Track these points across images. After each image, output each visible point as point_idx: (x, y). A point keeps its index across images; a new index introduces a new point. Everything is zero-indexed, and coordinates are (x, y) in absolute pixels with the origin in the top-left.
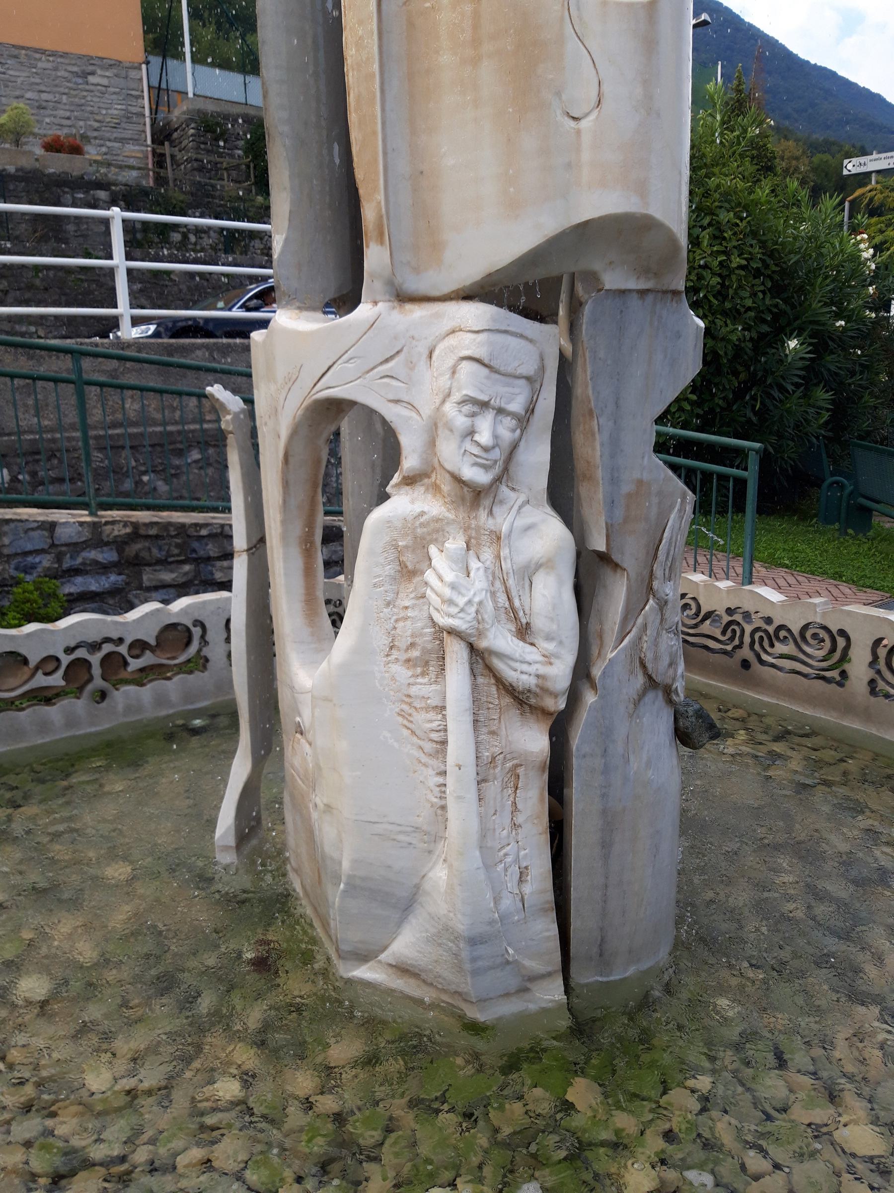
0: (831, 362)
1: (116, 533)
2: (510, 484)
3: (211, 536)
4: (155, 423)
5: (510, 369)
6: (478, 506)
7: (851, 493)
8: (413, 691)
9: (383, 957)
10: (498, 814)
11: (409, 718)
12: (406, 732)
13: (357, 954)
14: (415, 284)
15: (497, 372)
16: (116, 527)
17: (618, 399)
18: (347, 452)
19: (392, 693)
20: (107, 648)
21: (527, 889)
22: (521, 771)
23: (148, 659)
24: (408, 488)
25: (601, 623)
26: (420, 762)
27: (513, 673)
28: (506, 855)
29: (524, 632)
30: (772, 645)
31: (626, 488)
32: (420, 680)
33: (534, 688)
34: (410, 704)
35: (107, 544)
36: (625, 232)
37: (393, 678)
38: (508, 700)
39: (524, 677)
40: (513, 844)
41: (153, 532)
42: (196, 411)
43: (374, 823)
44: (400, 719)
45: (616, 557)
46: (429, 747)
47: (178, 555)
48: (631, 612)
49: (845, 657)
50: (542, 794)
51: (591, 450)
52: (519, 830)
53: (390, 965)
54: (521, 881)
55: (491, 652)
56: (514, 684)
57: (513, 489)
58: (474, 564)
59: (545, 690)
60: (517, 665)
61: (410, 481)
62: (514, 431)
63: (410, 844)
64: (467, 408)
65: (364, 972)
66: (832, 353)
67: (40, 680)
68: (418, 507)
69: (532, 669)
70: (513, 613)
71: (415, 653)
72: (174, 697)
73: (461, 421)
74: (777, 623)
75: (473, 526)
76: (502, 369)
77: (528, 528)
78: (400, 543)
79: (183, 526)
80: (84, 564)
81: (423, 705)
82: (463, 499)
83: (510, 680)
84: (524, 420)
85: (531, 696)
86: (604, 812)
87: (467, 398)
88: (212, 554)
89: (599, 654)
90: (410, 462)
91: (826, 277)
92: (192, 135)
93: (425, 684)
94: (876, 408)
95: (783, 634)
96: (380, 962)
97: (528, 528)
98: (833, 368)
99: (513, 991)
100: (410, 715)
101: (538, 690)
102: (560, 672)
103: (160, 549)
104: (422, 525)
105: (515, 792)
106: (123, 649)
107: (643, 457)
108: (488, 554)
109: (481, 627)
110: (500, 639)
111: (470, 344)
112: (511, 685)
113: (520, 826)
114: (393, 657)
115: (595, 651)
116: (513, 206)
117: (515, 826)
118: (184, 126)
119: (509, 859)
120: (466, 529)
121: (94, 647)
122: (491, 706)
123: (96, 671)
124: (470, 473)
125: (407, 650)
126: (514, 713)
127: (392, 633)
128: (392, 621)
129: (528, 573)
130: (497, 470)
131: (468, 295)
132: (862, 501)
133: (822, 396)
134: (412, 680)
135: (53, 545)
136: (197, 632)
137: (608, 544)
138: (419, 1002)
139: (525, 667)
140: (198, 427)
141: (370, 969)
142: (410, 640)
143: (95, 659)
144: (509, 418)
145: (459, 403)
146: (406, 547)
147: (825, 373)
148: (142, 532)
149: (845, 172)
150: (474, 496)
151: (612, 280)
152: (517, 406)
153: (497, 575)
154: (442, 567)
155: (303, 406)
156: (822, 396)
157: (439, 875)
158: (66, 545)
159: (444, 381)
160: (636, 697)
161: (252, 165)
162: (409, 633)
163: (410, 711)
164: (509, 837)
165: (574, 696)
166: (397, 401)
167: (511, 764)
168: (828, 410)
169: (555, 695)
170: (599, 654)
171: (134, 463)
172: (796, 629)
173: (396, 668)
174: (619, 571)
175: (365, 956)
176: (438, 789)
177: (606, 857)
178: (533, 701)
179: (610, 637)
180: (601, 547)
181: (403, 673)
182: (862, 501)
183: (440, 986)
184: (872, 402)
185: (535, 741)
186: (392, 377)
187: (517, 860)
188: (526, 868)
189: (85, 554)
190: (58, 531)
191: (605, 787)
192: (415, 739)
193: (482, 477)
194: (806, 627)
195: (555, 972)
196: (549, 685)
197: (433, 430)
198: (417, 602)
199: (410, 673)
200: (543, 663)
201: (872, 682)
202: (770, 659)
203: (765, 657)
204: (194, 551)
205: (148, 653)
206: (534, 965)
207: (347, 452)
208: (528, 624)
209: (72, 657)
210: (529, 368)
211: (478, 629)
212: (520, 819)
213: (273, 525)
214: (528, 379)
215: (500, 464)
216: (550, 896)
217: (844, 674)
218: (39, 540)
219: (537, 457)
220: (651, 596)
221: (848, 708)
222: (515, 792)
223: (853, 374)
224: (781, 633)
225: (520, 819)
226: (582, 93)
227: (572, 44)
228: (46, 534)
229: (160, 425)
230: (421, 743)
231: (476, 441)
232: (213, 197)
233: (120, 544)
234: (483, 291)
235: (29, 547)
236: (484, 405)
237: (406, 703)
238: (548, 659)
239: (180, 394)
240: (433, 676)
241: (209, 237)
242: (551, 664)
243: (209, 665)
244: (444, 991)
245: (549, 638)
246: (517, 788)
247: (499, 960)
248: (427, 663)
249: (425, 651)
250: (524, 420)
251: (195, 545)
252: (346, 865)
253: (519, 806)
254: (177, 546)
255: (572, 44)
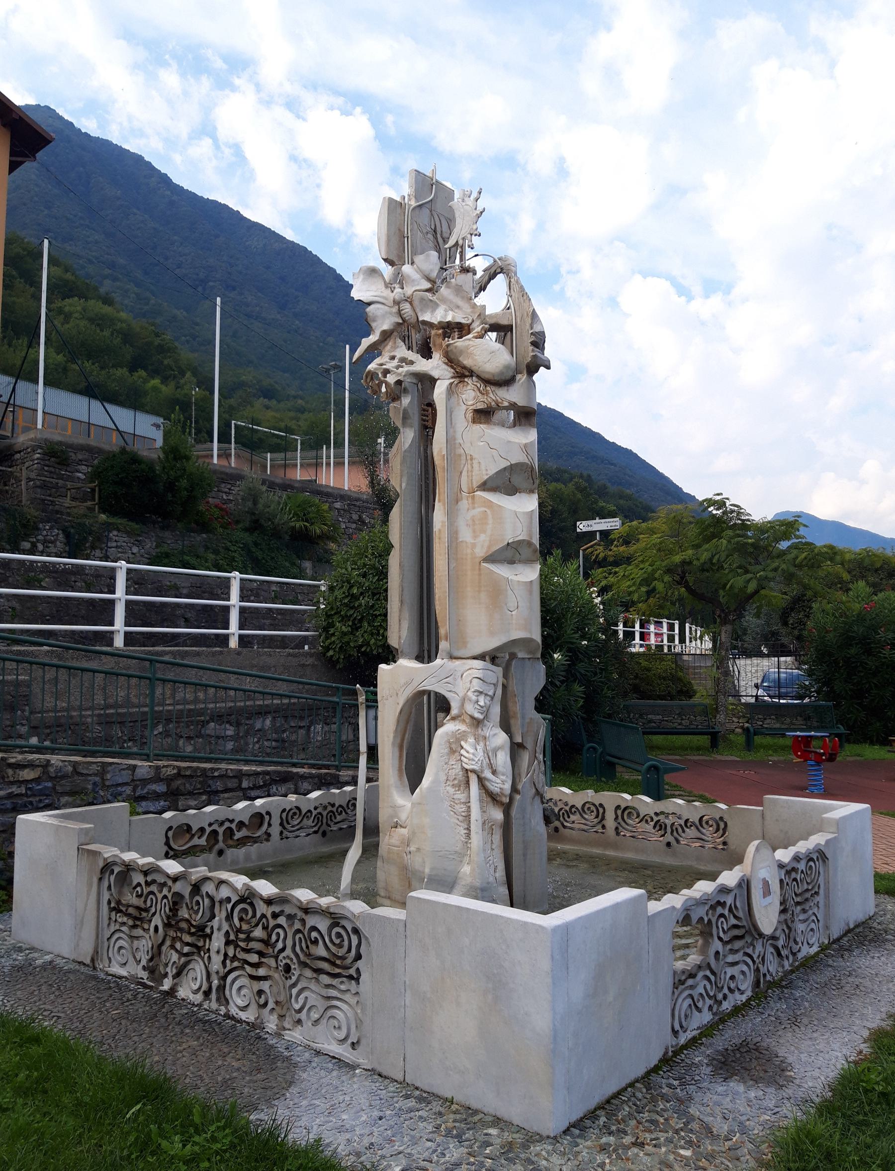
0: (581, 667)
1: (169, 773)
3: (220, 776)
4: (134, 706)
7: (602, 753)
8: (455, 797)
14: (456, 654)
16: (169, 769)
18: (431, 707)
20: (227, 824)
21: (497, 875)
23: (244, 832)
29: (494, 772)
30: (569, 817)
31: (527, 720)
35: (161, 780)
36: (524, 642)
38: (489, 799)
41: (188, 773)
42: (161, 697)
47: (199, 789)
48: (530, 764)
49: (603, 818)
51: (516, 708)
58: (478, 747)
61: (453, 719)
64: (476, 694)
66: (581, 661)
67: (196, 841)
69: (498, 786)
70: (491, 765)
71: (456, 782)
72: (254, 857)
73: (474, 698)
74: (570, 805)
77: (495, 735)
79: (205, 769)
80: (148, 793)
84: (492, 698)
88: (219, 789)
90: (454, 711)
91: (573, 614)
92: (38, 459)
94: (613, 698)
95: (573, 810)
97: (495, 735)
98: (583, 672)
102: (507, 787)
103: (191, 785)
106: (233, 826)
108: (482, 744)
110: (488, 774)
111: (479, 674)
115: (517, 780)
116: (492, 633)
117: (492, 849)
118: (29, 450)
121: (222, 824)
123: (221, 838)
124: (477, 715)
126: (491, 805)
127: (447, 775)
129: (495, 751)
131: (475, 658)
132: (609, 758)
133: (578, 688)
135: (133, 780)
136: (267, 817)
140: (83, 713)
143: (221, 830)
147: (578, 674)
148: (183, 773)
149: (578, 530)
150: (477, 723)
151: (520, 655)
152: (491, 693)
153: (486, 751)
154: (468, 745)
156: (578, 688)
157: (466, 869)
158: (139, 780)
159: (468, 685)
161: (97, 489)
165: (511, 798)
168: (582, 698)
171: (120, 735)
172: (579, 806)
173: (448, 788)
177: (525, 860)
179: (523, 775)
180: (520, 741)
181: (451, 790)
182: (609, 758)
184: (609, 694)
189: (149, 787)
190: (137, 770)
193: (481, 717)
194: (584, 805)
197: (463, 700)
200: (501, 784)
201: (617, 828)
202: (568, 825)
203: (566, 824)
204: (209, 786)
205: (244, 829)
209: (211, 829)
213: (386, 739)
217: (604, 827)
218: (125, 777)
221: (607, 845)
223: (595, 674)
224: (572, 809)
226: (512, 604)
227: (510, 592)
228: (130, 772)
229: (137, 707)
232: (62, 513)
233: (169, 780)
234: (481, 657)
235: (120, 781)
236: (481, 693)
238: (503, 782)
239: (226, 688)
241: (55, 547)
243: (271, 838)
245: (503, 775)
249: (460, 781)
251: (210, 782)
252: (427, 871)
254: (200, 783)
255: (510, 592)
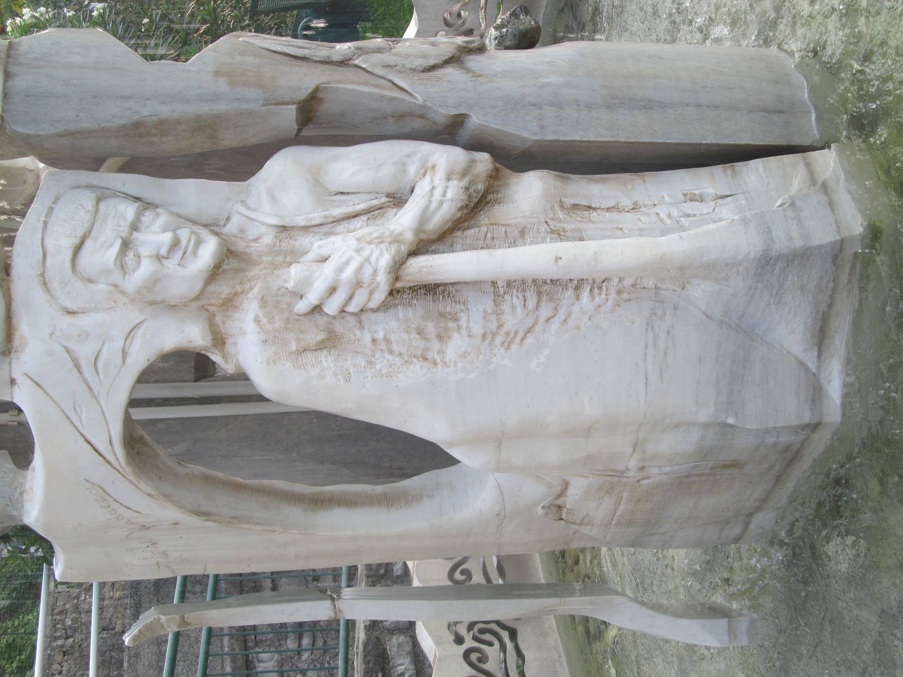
2: (222, 223)
5: (87, 218)
6: (245, 254)
8: (477, 330)
9: (812, 365)
10: (620, 226)
11: (512, 335)
12: (530, 340)
13: (813, 400)
15: (90, 231)
17: (122, 97)
19: (482, 357)
21: (710, 191)
22: (568, 202)
24: (229, 341)
25: (385, 117)
26: (565, 321)
27: (445, 206)
28: (669, 216)
29: (397, 200)
32: (463, 323)
33: (464, 183)
34: (494, 335)
37: (464, 355)
39: (450, 194)
40: (657, 210)
43: (647, 379)
44: (514, 347)
45: (303, 95)
46: (546, 310)
50: (596, 181)
52: (641, 203)
53: (819, 355)
54: (701, 199)
55: (419, 229)
56: (459, 205)
57: (228, 219)
59: (465, 173)
60: (434, 205)
62: (158, 215)
63: (668, 332)
65: (834, 389)
68: (249, 325)
75: (270, 259)
76: (86, 225)
78: (294, 348)
81: (494, 318)
82: (238, 270)
83: (454, 209)
85: (474, 188)
86: (609, 107)
87: (118, 262)
89: (421, 116)
93: (468, 316)
96: (819, 368)
99: (826, 199)
100: (507, 334)
101: (466, 179)
102: (445, 157)
104: (271, 320)
105: (595, 209)
107: (189, 71)
109: (388, 240)
112: (461, 209)
113: (635, 203)
114: (436, 356)
117: (635, 208)
119: (675, 213)
120: (274, 266)
122: (489, 235)
125: (427, 339)
128: (391, 358)
130: (204, 233)
134: (464, 332)
137: (288, 103)
138: (858, 314)
139: (438, 193)
141: (829, 382)
142: (414, 335)
144: (143, 219)
145: (125, 273)
146: (298, 341)
152: (129, 210)
155: (135, 482)
160: (470, 75)
162: (405, 336)
163: (503, 334)
164: (648, 214)
166: (125, 354)
167: (559, 213)
169: (473, 162)
170: (421, 116)
174: (320, 95)
175: (814, 389)
176: (597, 298)
178: (480, 187)
181: (456, 344)
183: (831, 285)
185: (530, 190)
186: (96, 359)
187: (676, 204)
188: (685, 195)
191: (578, 105)
192: (538, 328)
195: (804, 159)
196: (459, 168)
197: (153, 300)
198: (366, 327)
199: (456, 335)
200: (437, 177)
206: (797, 181)
207: (188, 416)
208: (388, 196)
210: (87, 199)
211: (390, 243)
212: (627, 203)
214: (99, 200)
215: (195, 228)
216: (717, 170)
219: (194, 193)
220: (351, 62)
222: (595, 209)
225: (627, 203)
230: (542, 319)
231: (169, 252)
237: (493, 339)
240: (458, 307)
242: (434, 167)
244: (836, 279)
246: (590, 207)
247: (790, 214)
248: (442, 315)
250: (146, 205)
253: (611, 204)
